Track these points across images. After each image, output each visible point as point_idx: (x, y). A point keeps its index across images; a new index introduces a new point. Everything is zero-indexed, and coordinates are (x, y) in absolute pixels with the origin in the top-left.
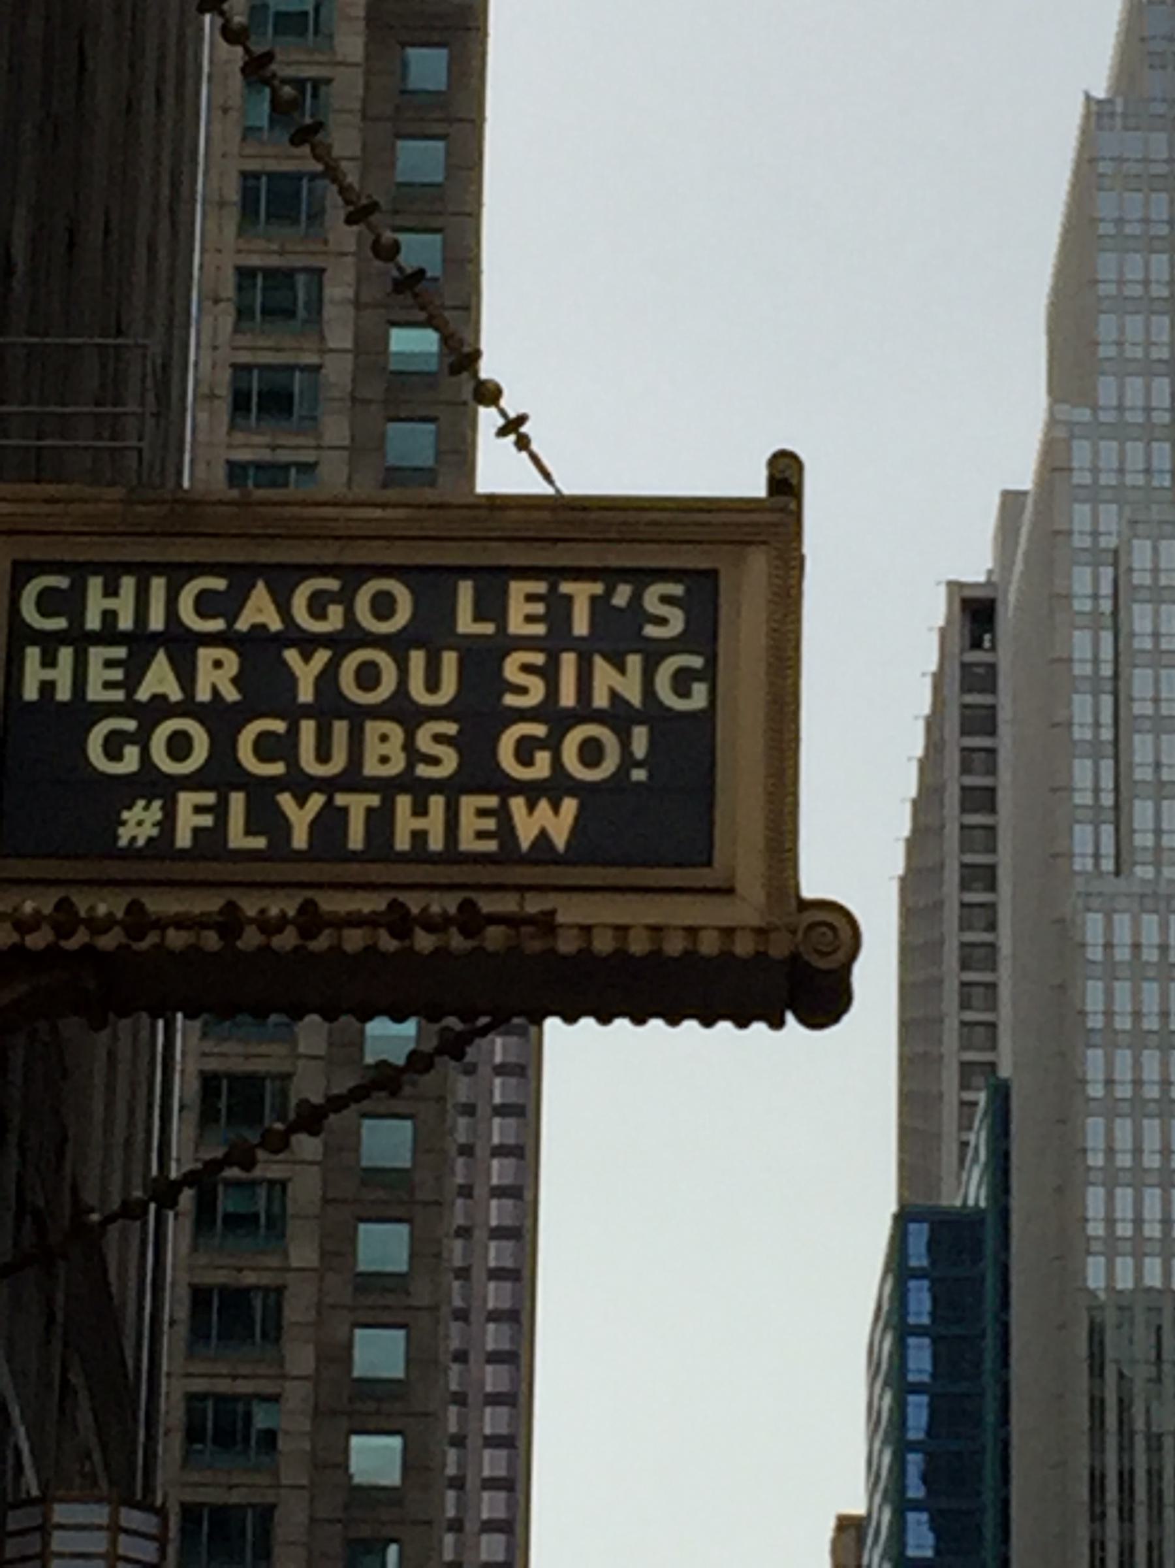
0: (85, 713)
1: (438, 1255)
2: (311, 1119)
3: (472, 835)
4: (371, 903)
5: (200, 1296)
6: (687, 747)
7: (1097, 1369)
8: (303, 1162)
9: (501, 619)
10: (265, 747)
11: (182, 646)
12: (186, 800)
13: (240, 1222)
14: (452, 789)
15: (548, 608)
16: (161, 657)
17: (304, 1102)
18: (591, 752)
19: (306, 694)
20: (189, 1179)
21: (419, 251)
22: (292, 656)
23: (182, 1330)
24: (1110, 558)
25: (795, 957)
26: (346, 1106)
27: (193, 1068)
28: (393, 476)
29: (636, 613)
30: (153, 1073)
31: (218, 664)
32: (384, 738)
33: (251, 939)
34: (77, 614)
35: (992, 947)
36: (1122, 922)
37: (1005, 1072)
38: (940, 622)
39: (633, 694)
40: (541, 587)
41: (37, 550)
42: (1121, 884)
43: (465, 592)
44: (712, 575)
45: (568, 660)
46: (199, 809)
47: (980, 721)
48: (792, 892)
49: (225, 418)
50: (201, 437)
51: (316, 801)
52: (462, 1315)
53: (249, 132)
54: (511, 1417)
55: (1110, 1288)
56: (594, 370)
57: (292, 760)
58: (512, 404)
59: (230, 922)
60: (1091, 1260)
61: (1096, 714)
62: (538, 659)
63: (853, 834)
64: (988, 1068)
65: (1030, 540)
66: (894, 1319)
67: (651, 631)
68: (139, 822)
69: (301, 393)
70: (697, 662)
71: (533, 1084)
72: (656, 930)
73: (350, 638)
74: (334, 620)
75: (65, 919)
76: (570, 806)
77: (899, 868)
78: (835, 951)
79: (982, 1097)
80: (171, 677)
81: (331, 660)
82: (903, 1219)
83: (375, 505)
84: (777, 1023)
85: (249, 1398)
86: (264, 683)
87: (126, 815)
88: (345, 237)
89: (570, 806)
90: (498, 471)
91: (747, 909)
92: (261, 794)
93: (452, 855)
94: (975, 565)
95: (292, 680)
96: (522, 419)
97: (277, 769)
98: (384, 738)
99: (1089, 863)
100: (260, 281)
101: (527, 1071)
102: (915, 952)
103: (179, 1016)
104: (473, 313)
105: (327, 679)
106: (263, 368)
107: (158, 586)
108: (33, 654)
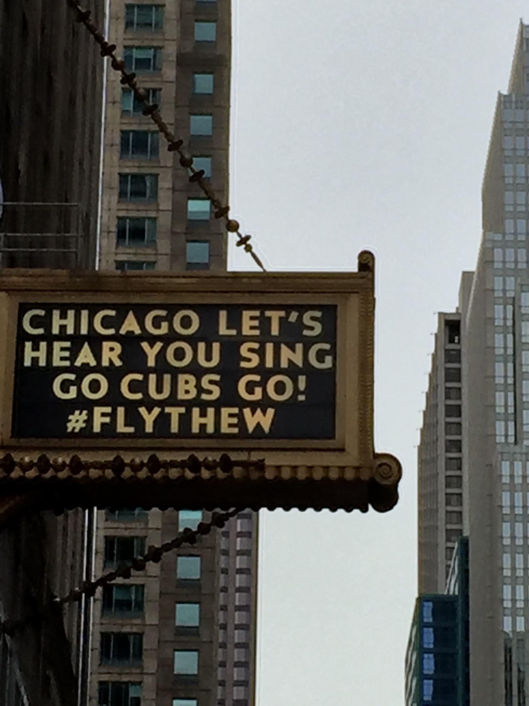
0: (52, 372)
1: (213, 618)
2: (155, 555)
3: (226, 425)
4: (182, 457)
5: (105, 637)
6: (323, 384)
7: (508, 669)
8: (151, 576)
9: (239, 328)
10: (133, 387)
11: (95, 341)
12: (98, 411)
13: (124, 605)
14: (218, 405)
15: (260, 323)
16: (86, 346)
17: (151, 547)
18: (280, 388)
19: (151, 363)
20: (101, 582)
21: (200, 164)
22: (145, 345)
23: (97, 653)
24: (511, 301)
25: (372, 480)
26: (170, 549)
27: (102, 533)
28: (190, 266)
29: (300, 325)
30: (78, 661)
31: (112, 349)
32: (187, 382)
33: (127, 473)
34: (48, 326)
35: (460, 477)
36: (518, 465)
37: (466, 533)
38: (435, 330)
39: (299, 361)
40: (257, 313)
41: (31, 299)
42: (517, 449)
43: (223, 315)
44: (335, 307)
45: (269, 347)
46: (103, 415)
47: (454, 375)
48: (371, 450)
49: (115, 241)
50: (103, 251)
51: (156, 411)
52: (223, 646)
53: (124, 113)
54: (245, 690)
55: (514, 631)
56: (280, 220)
57: (146, 394)
58: (243, 231)
59: (118, 466)
60: (505, 587)
61: (506, 370)
62: (256, 346)
63: (398, 423)
64: (459, 514)
65: (476, 286)
66: (417, 645)
67: (306, 332)
68: (76, 421)
69: (149, 230)
70: (327, 347)
71: (255, 523)
72: (310, 468)
73: (171, 337)
74: (164, 329)
75: (43, 465)
76: (271, 412)
77: (418, 442)
78: (390, 477)
79: (456, 545)
80: (91, 355)
81: (163, 347)
82: (421, 600)
83: (184, 277)
84: (364, 510)
85: (127, 683)
86: (133, 357)
87: (71, 417)
88: (167, 158)
89: (271, 412)
90: (238, 261)
91: (351, 458)
92: (132, 408)
93: (217, 434)
94: (451, 305)
95: (145, 356)
96: (248, 238)
97: (139, 396)
98: (187, 382)
99: (503, 440)
100: (136, 10)
101: (251, 535)
102: (424, 480)
103: (95, 509)
104: (225, 193)
105: (161, 356)
106: (131, 219)
107: (85, 314)
108: (28, 345)
